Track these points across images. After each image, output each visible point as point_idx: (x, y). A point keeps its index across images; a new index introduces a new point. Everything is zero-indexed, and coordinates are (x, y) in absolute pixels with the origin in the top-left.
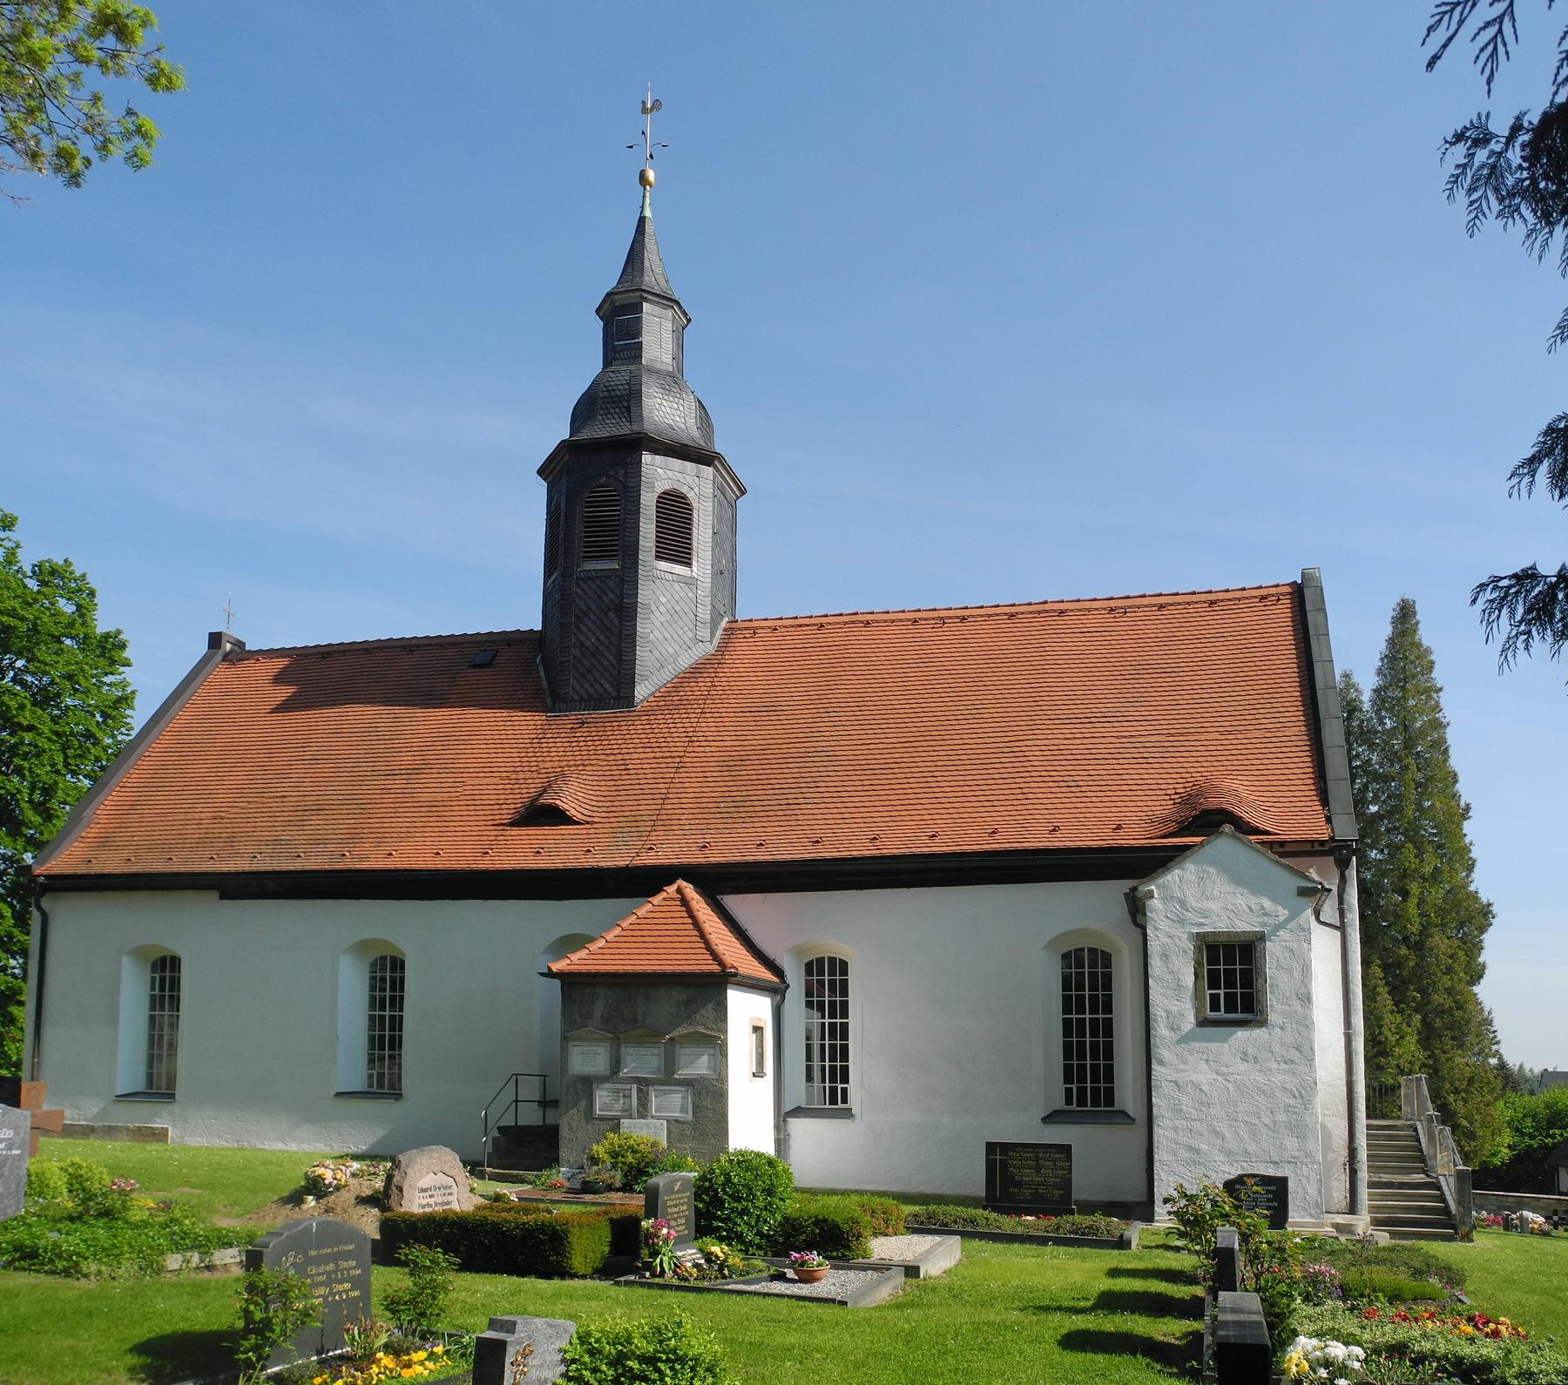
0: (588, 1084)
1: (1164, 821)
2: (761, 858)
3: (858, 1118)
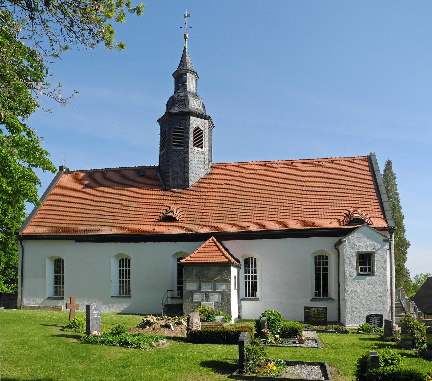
0: (191, 293)
1: (343, 221)
2: (234, 231)
3: (260, 301)
